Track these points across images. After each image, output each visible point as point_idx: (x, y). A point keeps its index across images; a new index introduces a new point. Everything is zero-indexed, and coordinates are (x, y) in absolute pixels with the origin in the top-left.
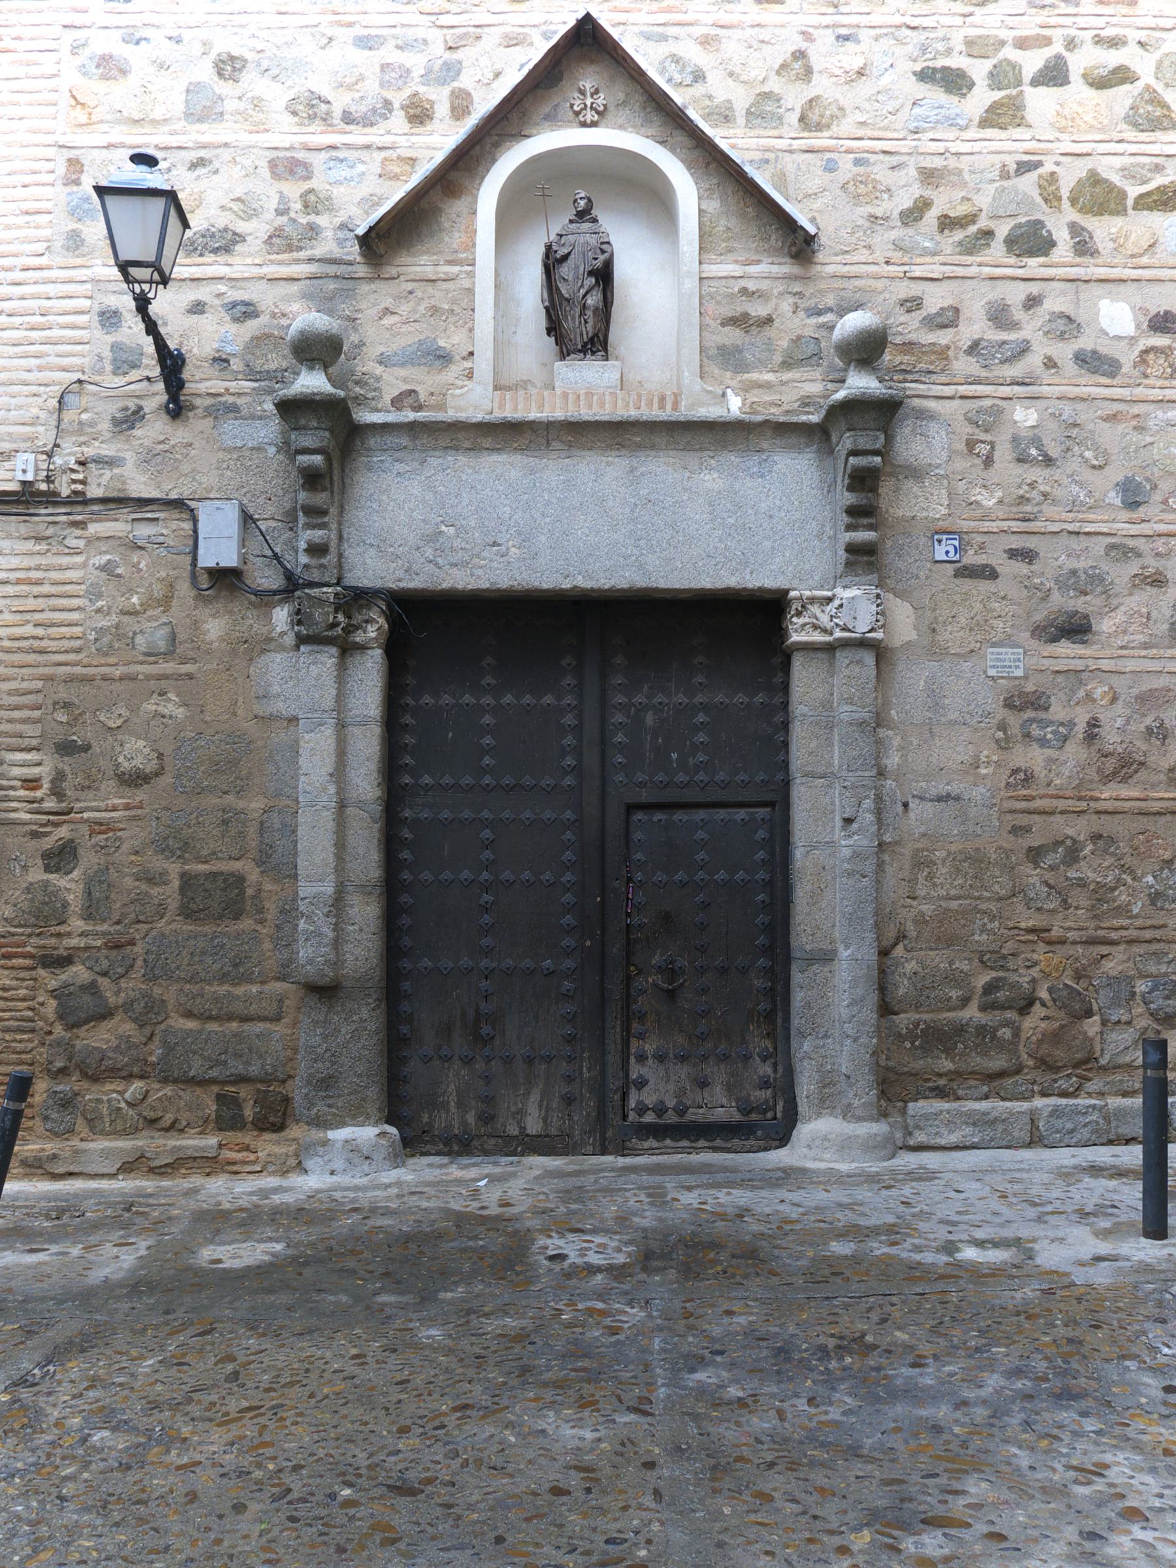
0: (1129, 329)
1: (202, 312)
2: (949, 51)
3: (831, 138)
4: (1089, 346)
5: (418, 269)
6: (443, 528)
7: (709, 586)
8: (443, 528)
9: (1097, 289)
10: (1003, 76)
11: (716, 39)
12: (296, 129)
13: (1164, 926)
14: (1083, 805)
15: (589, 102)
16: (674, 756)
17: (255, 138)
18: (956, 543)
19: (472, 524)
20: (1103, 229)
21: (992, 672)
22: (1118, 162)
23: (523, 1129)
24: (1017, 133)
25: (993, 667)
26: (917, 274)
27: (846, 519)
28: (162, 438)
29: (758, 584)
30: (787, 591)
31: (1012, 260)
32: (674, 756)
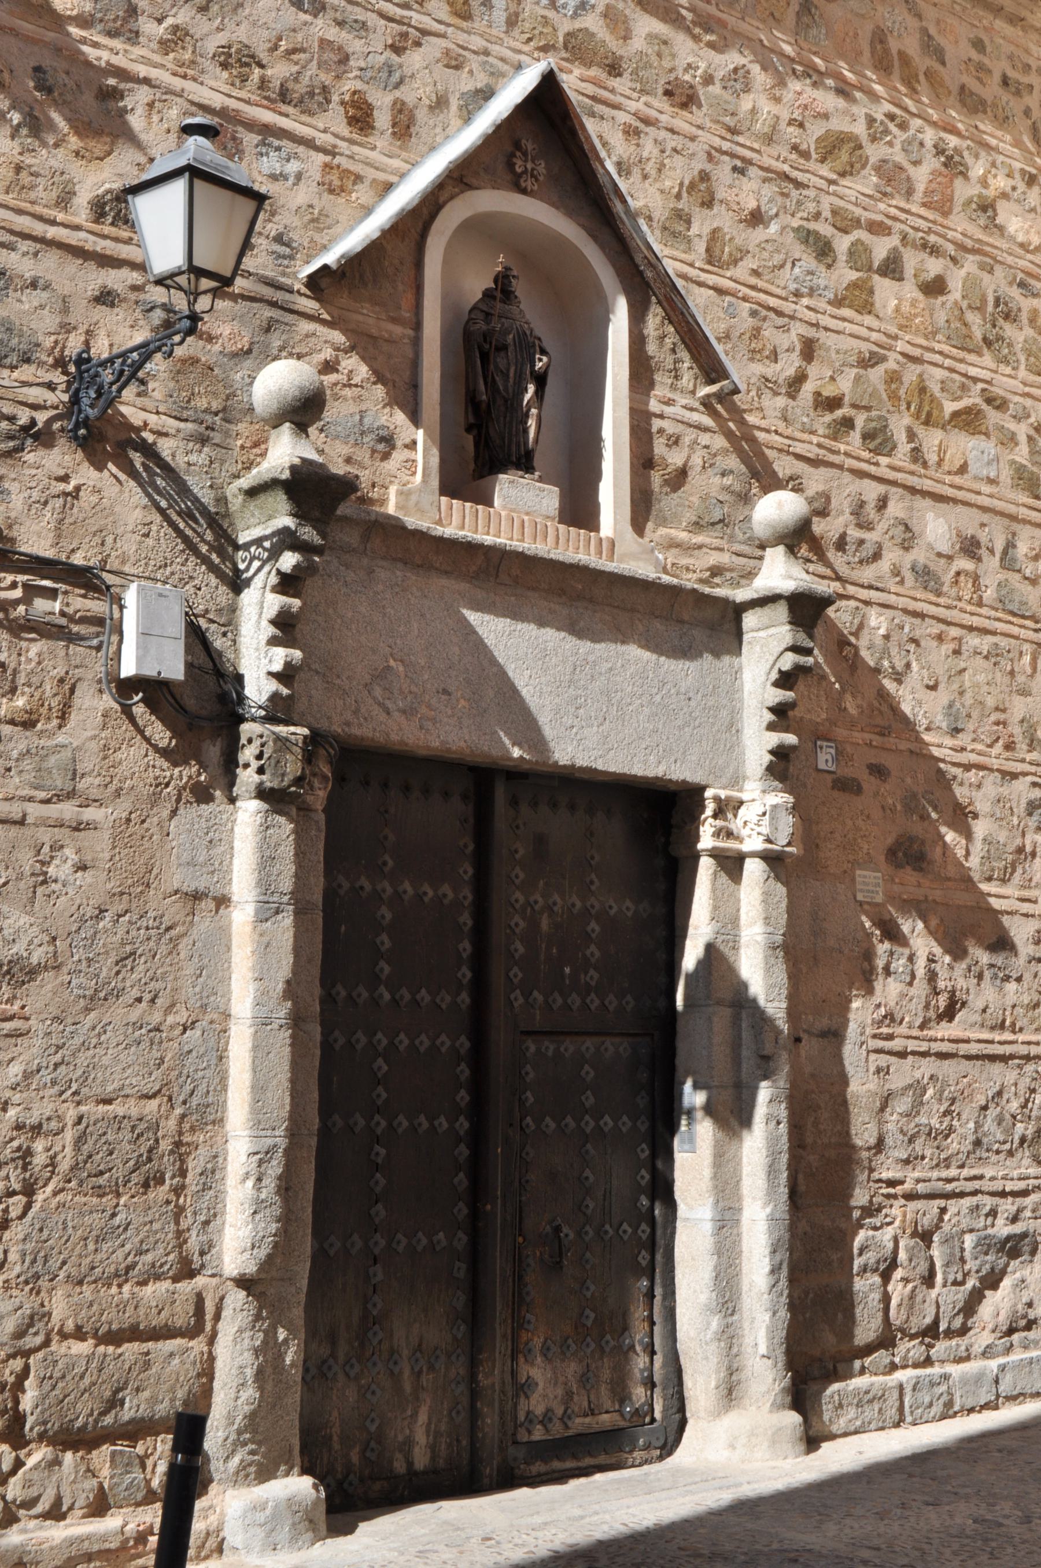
0: (944, 548)
1: (112, 305)
2: (817, 216)
3: (731, 279)
4: (922, 560)
5: (360, 318)
6: (392, 663)
7: (640, 773)
8: (392, 663)
9: (928, 502)
10: (858, 255)
11: (637, 132)
12: (226, 88)
13: (981, 1177)
14: (924, 1047)
15: (529, 166)
16: (567, 970)
17: (177, 83)
18: (833, 751)
19: (422, 662)
20: (932, 439)
21: (860, 897)
22: (678, 265)
23: (410, 1464)
24: (869, 320)
25: (861, 891)
26: (798, 451)
27: (769, 717)
28: (61, 472)
29: (682, 778)
30: (702, 789)
31: (866, 455)
32: (567, 970)
